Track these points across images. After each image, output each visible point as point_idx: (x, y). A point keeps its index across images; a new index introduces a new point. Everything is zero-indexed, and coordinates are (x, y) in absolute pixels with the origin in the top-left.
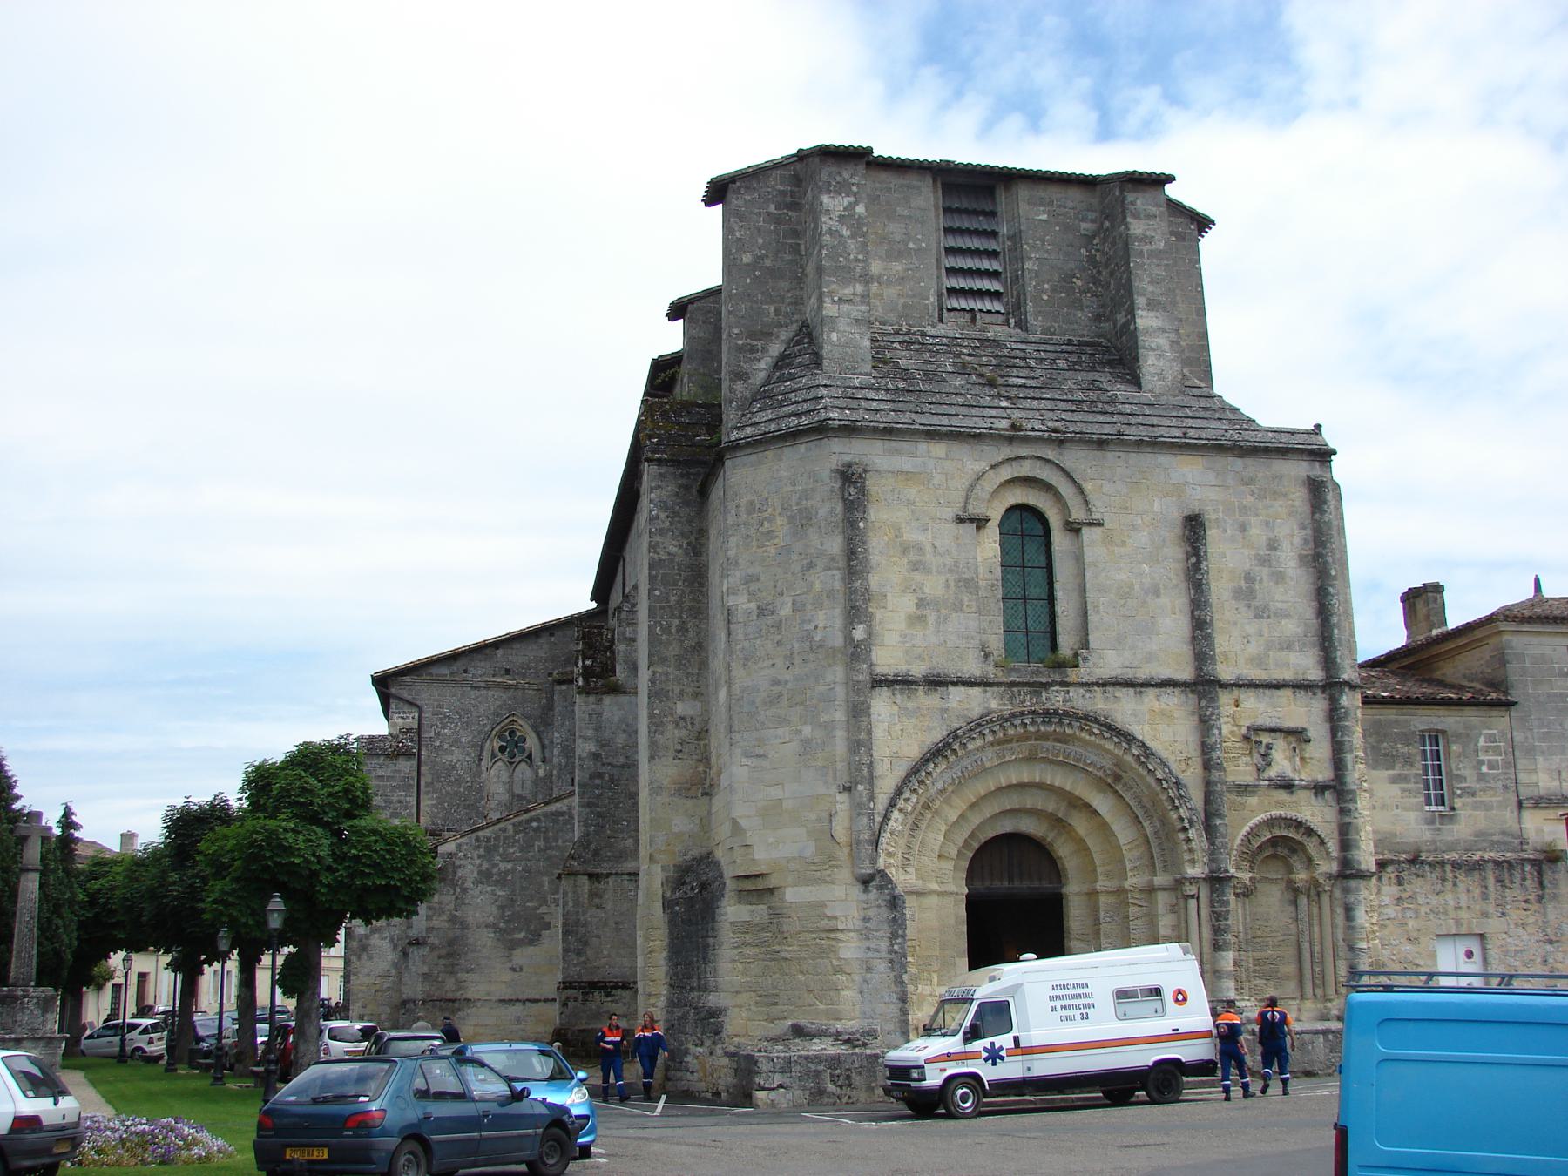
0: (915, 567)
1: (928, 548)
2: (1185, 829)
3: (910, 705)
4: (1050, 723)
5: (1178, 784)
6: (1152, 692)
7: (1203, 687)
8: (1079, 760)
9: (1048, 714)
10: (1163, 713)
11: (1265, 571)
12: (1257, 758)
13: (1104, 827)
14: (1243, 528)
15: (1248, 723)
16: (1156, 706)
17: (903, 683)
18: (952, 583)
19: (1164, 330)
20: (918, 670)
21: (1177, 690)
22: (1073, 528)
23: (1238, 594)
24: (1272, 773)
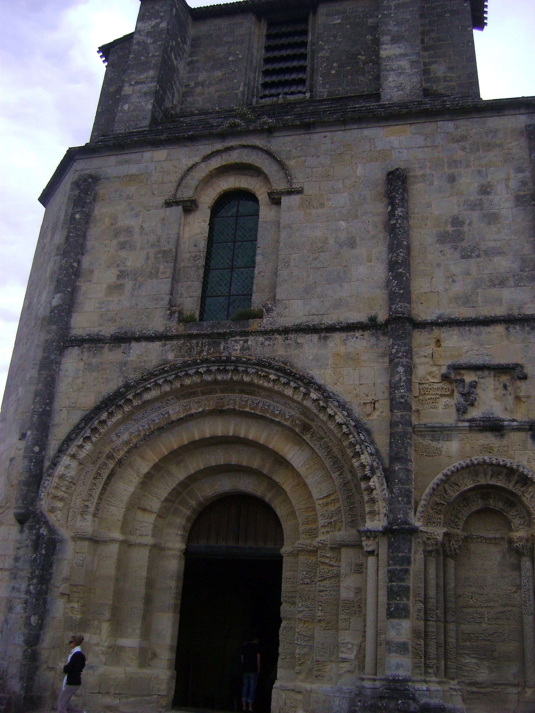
1: (137, 230)
2: (367, 478)
3: (94, 361)
4: (226, 371)
5: (359, 427)
6: (337, 337)
7: (397, 326)
8: (267, 411)
11: (475, 215)
13: (302, 484)
14: (452, 179)
15: (450, 362)
17: (94, 342)
18: (152, 255)
19: (405, 55)
20: (108, 330)
22: (275, 200)
23: (443, 238)
24: (475, 413)
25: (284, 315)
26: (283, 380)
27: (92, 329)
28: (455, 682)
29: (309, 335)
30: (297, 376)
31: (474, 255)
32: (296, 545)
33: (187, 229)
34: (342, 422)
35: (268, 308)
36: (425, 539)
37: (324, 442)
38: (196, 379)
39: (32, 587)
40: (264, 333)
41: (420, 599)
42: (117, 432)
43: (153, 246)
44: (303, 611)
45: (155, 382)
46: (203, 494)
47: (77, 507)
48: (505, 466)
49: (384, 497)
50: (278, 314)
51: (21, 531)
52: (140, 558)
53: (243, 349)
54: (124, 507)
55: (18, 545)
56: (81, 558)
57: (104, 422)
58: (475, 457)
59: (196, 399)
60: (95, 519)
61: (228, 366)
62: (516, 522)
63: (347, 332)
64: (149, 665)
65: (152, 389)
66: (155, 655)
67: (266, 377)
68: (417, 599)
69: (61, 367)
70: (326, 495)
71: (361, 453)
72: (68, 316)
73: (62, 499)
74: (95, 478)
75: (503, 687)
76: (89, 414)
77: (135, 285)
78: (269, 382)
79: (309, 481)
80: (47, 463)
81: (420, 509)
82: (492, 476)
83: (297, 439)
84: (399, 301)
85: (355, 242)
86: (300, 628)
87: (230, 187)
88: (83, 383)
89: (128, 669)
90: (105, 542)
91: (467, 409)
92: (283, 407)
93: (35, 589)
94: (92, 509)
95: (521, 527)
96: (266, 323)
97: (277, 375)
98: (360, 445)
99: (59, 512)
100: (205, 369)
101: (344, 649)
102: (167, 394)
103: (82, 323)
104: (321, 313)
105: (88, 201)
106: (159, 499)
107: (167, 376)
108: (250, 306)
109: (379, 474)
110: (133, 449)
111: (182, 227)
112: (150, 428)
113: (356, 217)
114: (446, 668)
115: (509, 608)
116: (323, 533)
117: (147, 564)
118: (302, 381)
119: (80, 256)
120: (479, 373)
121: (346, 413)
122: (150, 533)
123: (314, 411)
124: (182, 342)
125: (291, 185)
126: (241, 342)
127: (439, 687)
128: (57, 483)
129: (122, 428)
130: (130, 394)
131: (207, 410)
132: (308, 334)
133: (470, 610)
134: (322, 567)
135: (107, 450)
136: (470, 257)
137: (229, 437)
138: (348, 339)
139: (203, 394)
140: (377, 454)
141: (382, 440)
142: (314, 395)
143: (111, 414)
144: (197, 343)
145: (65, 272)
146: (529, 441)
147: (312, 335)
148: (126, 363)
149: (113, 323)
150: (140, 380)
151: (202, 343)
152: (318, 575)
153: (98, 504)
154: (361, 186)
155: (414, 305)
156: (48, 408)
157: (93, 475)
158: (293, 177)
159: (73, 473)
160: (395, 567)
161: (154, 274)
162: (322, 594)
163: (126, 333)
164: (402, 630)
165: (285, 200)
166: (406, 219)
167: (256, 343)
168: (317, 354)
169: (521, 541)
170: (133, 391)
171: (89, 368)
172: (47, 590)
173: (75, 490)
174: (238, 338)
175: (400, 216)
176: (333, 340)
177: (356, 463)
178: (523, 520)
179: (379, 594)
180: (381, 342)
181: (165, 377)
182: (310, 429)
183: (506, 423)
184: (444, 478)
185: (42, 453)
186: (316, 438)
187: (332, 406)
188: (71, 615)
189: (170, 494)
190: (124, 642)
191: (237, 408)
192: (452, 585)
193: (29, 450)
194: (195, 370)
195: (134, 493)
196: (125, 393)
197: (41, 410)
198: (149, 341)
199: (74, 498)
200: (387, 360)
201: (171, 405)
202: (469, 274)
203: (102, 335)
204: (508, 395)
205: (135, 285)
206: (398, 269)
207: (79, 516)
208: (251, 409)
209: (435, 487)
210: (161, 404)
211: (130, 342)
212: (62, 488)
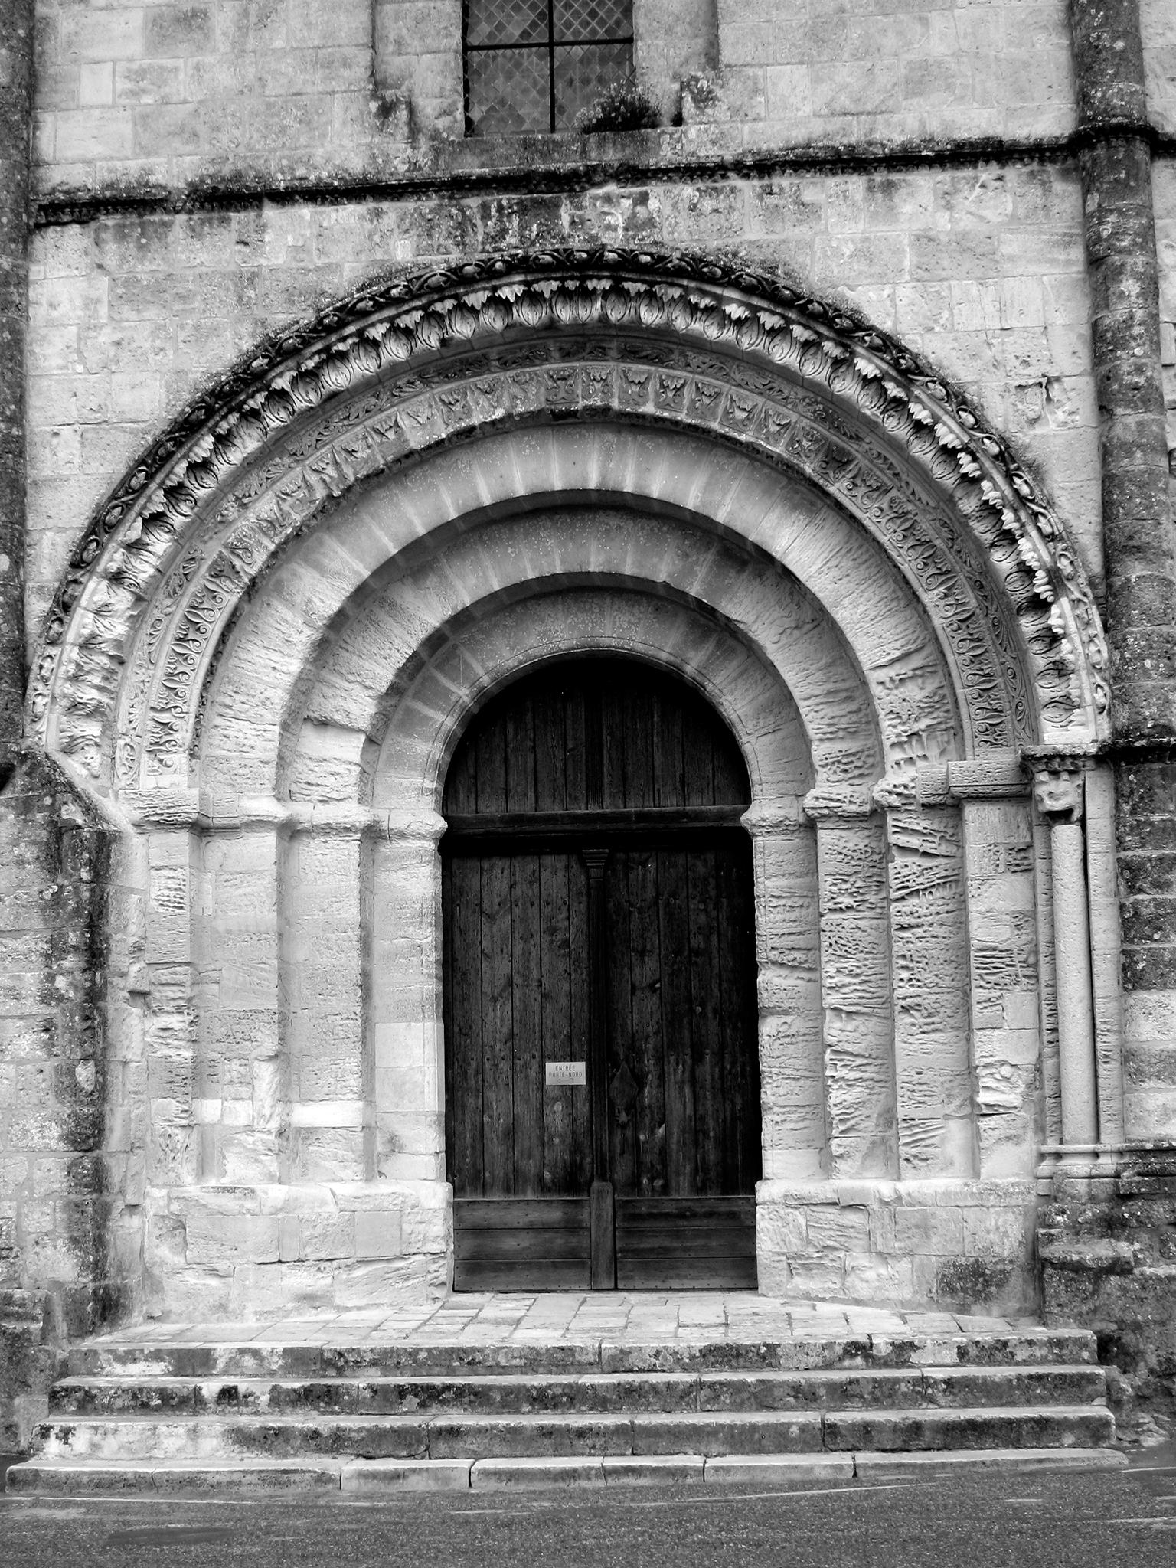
2: (1039, 606)
3: (145, 270)
4: (588, 296)
5: (1007, 459)
6: (924, 182)
9: (578, 270)
10: (963, 245)
13: (816, 621)
16: (943, 223)
17: (132, 205)
20: (174, 169)
21: (1014, 173)
25: (752, 114)
26: (769, 320)
27: (118, 164)
32: (809, 801)
34: (956, 443)
35: (701, 91)
37: (892, 501)
38: (493, 321)
39: (61, 982)
42: (239, 493)
44: (844, 986)
45: (360, 333)
46: (491, 664)
47: (138, 731)
50: (734, 111)
53: (631, 225)
54: (278, 720)
56: (172, 884)
57: (205, 466)
59: (483, 381)
61: (591, 278)
63: (952, 168)
64: (381, 1174)
65: (352, 356)
66: (394, 1145)
69: (32, 294)
70: (898, 654)
71: (1018, 533)
72: (27, 124)
74: (181, 640)
76: (158, 444)
77: (245, 13)
78: (722, 327)
79: (843, 615)
80: (37, 607)
83: (808, 495)
84: (1115, 76)
88: (118, 343)
90: (231, 830)
92: (760, 400)
93: (73, 985)
94: (184, 735)
96: (697, 140)
97: (749, 306)
98: (1015, 511)
99: (92, 752)
100: (519, 290)
101: (992, 1083)
102: (396, 369)
104: (869, 107)
106: (367, 688)
107: (398, 316)
108: (632, 84)
110: (295, 545)
112: (343, 477)
116: (898, 764)
121: (971, 420)
122: (353, 791)
128: (78, 665)
129: (254, 480)
130: (280, 375)
131: (520, 415)
132: (834, 174)
135: (212, 550)
137: (586, 491)
138: (957, 191)
139: (505, 365)
143: (224, 441)
147: (847, 178)
148: (252, 278)
149: (187, 143)
150: (314, 330)
151: (500, 208)
152: (893, 883)
155: (1151, 84)
156: (15, 432)
157: (173, 632)
159: (119, 628)
162: (907, 934)
163: (238, 176)
167: (674, 206)
168: (867, 239)
170: (291, 363)
174: (612, 188)
176: (912, 194)
177: (1002, 561)
179: (1094, 926)
180: (1057, 201)
181: (391, 320)
182: (849, 462)
185: (18, 576)
186: (864, 490)
187: (923, 397)
188: (166, 1051)
191: (615, 404)
194: (488, 294)
196: (265, 372)
198: (323, 203)
200: (1077, 254)
201: (403, 401)
203: (157, 186)
205: (245, 13)
207: (145, 756)
208: (657, 405)
210: (373, 401)
211: (260, 207)
212: (89, 677)
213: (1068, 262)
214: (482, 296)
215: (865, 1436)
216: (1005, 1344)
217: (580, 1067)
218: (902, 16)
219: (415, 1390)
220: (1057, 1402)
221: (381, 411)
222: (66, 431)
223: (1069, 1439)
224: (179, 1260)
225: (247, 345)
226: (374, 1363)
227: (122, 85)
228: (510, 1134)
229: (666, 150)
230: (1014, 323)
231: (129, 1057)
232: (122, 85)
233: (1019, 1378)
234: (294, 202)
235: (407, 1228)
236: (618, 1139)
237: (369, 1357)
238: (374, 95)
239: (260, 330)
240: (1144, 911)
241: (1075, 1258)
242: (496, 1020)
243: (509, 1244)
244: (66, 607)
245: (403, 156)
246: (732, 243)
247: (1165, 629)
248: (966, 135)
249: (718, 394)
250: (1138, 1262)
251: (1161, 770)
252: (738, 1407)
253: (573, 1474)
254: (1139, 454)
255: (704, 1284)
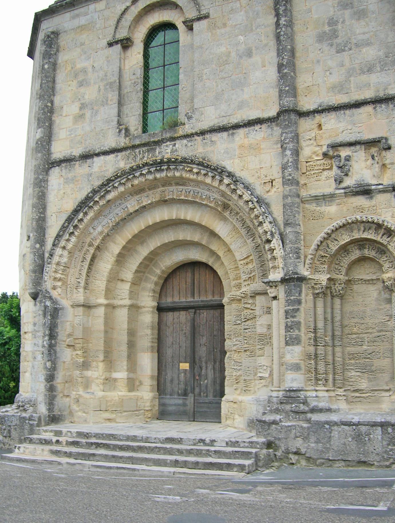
0: (81, 84)
1: (90, 69)
2: (269, 241)
3: (70, 175)
5: (260, 201)
6: (241, 131)
10: (251, 147)
11: (347, 13)
12: (335, 171)
15: (329, 142)
17: (68, 161)
18: (102, 88)
20: (77, 152)
21: (264, 126)
23: (321, 38)
24: (348, 182)
25: (201, 120)
27: (66, 152)
28: (342, 390)
29: (221, 134)
30: (212, 167)
31: (346, 48)
33: (127, 62)
36: (313, 285)
39: (45, 343)
40: (186, 136)
41: (311, 330)
43: (102, 80)
45: (113, 185)
46: (164, 264)
48: (373, 222)
49: (281, 255)
51: (35, 305)
52: (122, 316)
53: (172, 151)
54: (106, 280)
55: (35, 315)
56: (79, 320)
57: (81, 220)
58: (349, 217)
59: (145, 194)
60: (86, 291)
62: (386, 265)
66: (141, 383)
67: (191, 171)
68: (309, 330)
73: (60, 280)
75: (379, 392)
80: (47, 255)
81: (308, 262)
82: (364, 231)
84: (285, 97)
85: (251, 52)
86: (236, 356)
87: (156, 22)
89: (120, 393)
91: (342, 179)
92: (208, 193)
94: (82, 284)
95: (390, 269)
96: (188, 129)
100: (146, 171)
103: (59, 149)
105: (53, 52)
109: (277, 238)
110: (107, 237)
111: (122, 61)
112: (116, 220)
113: (252, 30)
114: (334, 380)
115: (384, 333)
117: (127, 319)
118: (216, 171)
119: (52, 97)
120: (352, 148)
122: (127, 297)
123: (228, 193)
124: (128, 152)
125: (199, 12)
126: (171, 146)
127: (326, 394)
129: (96, 222)
133: (354, 336)
134: (245, 311)
135: (88, 240)
136: (344, 51)
138: (250, 133)
140: (274, 222)
141: (278, 211)
142: (226, 181)
143: (86, 214)
144: (140, 151)
145: (42, 111)
146: (393, 199)
147: (223, 133)
148: (91, 175)
151: (143, 151)
153: (86, 280)
154: (254, 3)
155: (300, 98)
156: (42, 215)
157: (81, 260)
158: (201, 5)
159: (65, 260)
160: (289, 308)
161: (105, 103)
164: (295, 354)
165: (196, 26)
166: (290, 26)
169: (390, 280)
170: (98, 194)
171: (67, 181)
172: (56, 343)
173: (69, 271)
174: (168, 143)
175: (284, 24)
178: (391, 263)
181: (120, 181)
183: (373, 187)
184: (326, 236)
189: (139, 267)
190: (115, 375)
192: (338, 318)
193: (33, 247)
195: (112, 269)
197: (37, 217)
199: (69, 278)
202: (343, 66)
204: (376, 163)
205: (92, 113)
206: (283, 70)
207: (75, 290)
208: (185, 197)
209: (319, 244)
213: (277, 148)
214: (139, 173)
215: (185, 464)
216: (238, 442)
217: (188, 364)
218: (237, 90)
219: (95, 443)
220: (242, 459)
221: (123, 204)
222: (54, 214)
223: (235, 469)
224: (78, 409)
225: (89, 191)
226: (94, 436)
227: (68, 133)
228: (172, 381)
229: (181, 131)
230: (263, 166)
231: (65, 360)
232: (68, 133)
233: (233, 451)
234: (100, 156)
235: (139, 404)
236: (196, 383)
237: (93, 435)
238: (118, 128)
239: (92, 187)
240: (288, 324)
241: (264, 419)
242: (169, 352)
243: (170, 408)
244: (51, 255)
245: (123, 141)
246: (195, 153)
247: (296, 245)
248: (252, 118)
249: (199, 192)
250: (281, 421)
251: (294, 285)
252: (164, 454)
253: (110, 468)
254: (289, 198)
255: (211, 421)
